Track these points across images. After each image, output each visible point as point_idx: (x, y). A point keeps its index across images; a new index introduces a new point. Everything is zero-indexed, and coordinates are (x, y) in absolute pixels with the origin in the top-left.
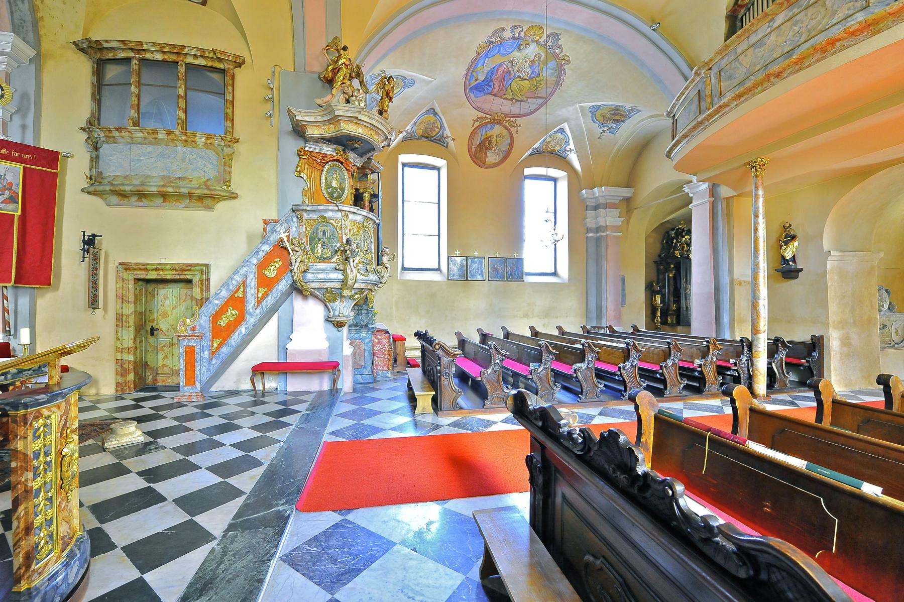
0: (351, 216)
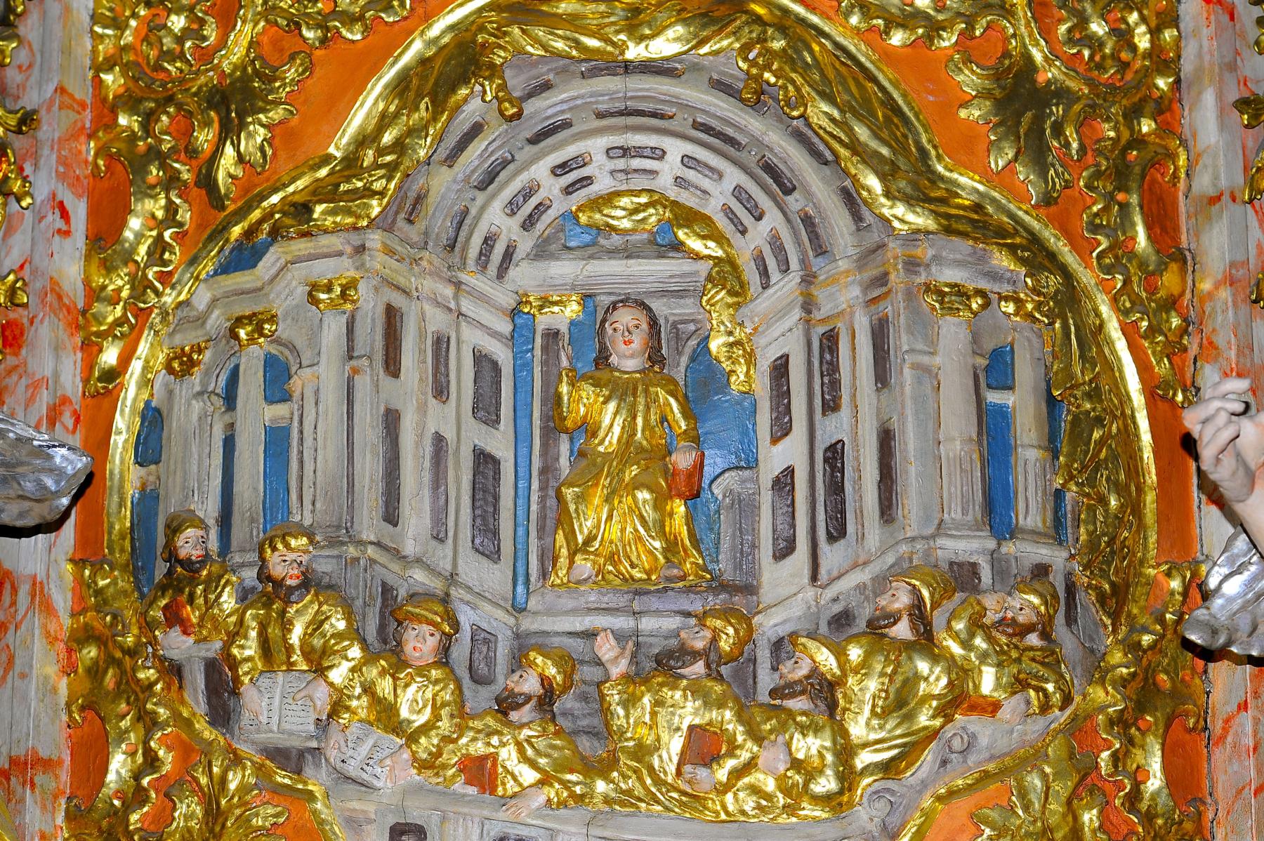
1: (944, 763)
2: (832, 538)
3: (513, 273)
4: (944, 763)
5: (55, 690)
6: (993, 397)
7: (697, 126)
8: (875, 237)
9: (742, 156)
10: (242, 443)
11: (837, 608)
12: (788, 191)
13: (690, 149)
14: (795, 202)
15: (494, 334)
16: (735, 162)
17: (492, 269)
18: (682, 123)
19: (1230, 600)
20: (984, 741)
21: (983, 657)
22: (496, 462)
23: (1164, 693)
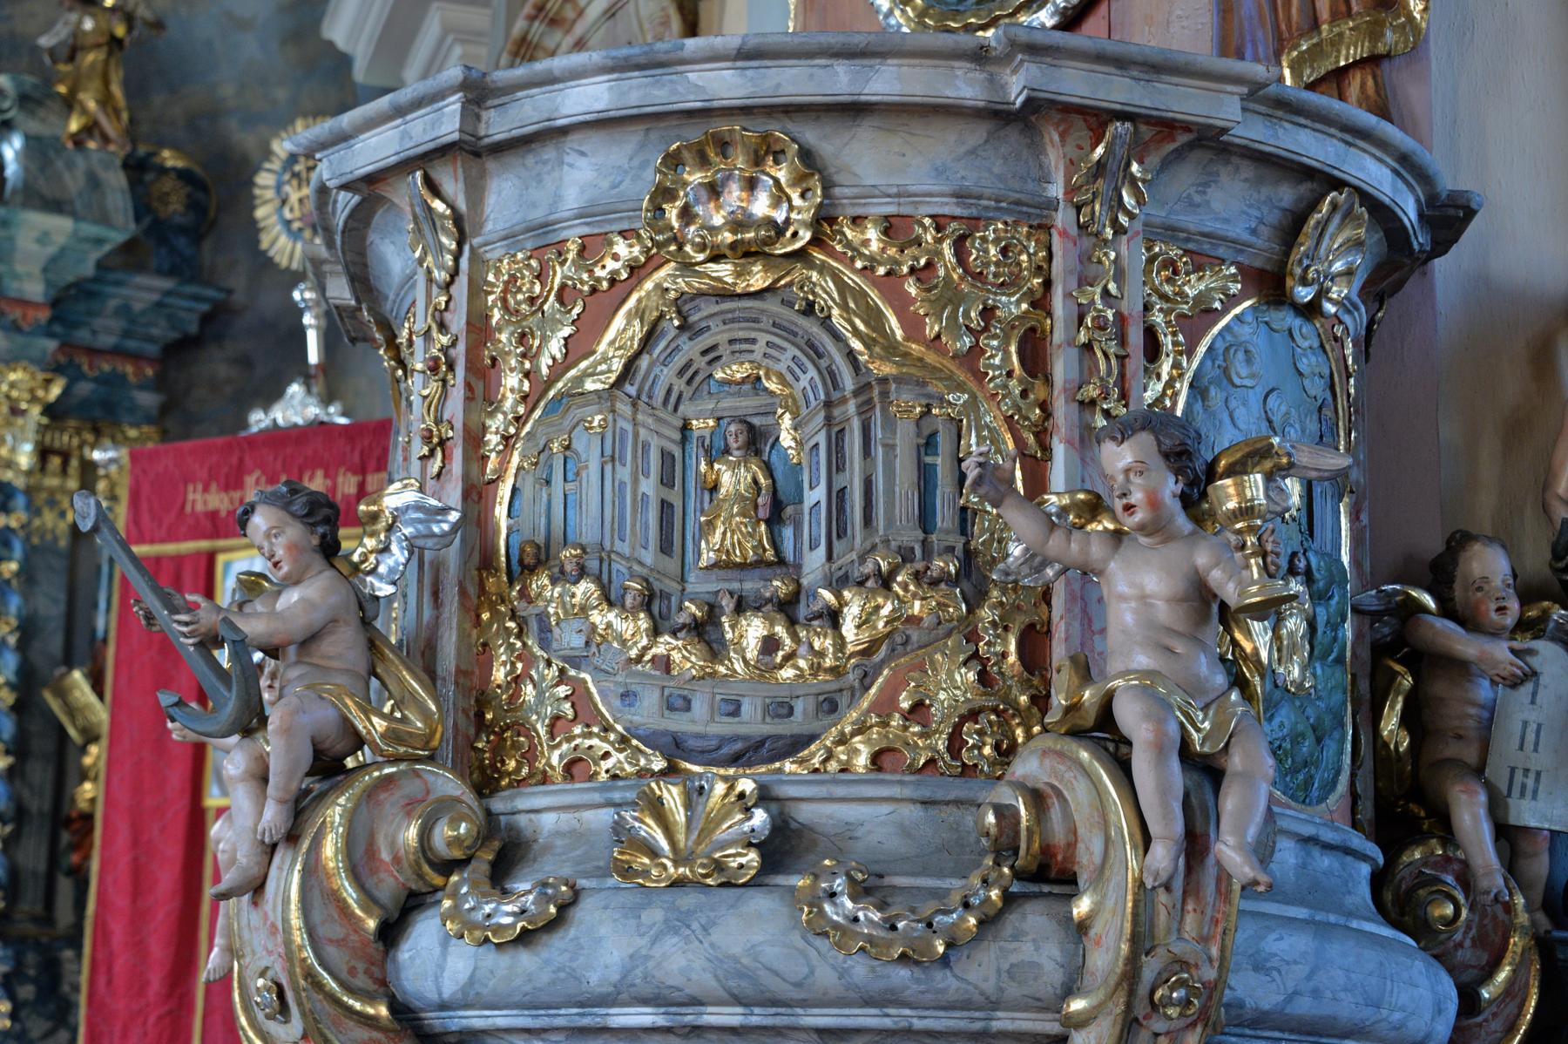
0: (505, 199)
1: (893, 650)
2: (839, 537)
3: (681, 408)
4: (893, 650)
5: (470, 636)
6: (928, 460)
7: (774, 325)
8: (864, 380)
9: (798, 340)
10: (554, 502)
11: (841, 573)
12: (820, 356)
13: (798, 353)
14: (823, 363)
15: (673, 441)
16: (760, 330)
17: (670, 407)
18: (766, 323)
19: (1016, 558)
20: (914, 638)
21: (915, 596)
22: (671, 506)
23: (1301, 479)
